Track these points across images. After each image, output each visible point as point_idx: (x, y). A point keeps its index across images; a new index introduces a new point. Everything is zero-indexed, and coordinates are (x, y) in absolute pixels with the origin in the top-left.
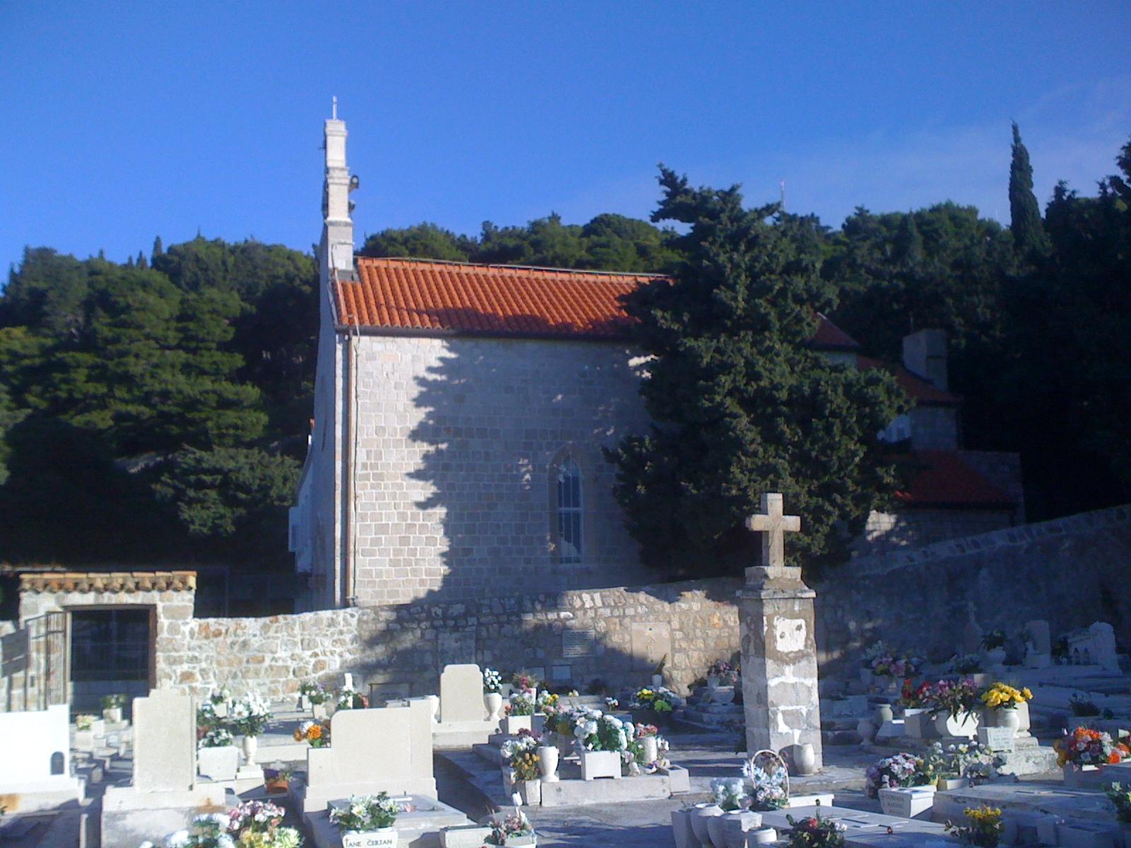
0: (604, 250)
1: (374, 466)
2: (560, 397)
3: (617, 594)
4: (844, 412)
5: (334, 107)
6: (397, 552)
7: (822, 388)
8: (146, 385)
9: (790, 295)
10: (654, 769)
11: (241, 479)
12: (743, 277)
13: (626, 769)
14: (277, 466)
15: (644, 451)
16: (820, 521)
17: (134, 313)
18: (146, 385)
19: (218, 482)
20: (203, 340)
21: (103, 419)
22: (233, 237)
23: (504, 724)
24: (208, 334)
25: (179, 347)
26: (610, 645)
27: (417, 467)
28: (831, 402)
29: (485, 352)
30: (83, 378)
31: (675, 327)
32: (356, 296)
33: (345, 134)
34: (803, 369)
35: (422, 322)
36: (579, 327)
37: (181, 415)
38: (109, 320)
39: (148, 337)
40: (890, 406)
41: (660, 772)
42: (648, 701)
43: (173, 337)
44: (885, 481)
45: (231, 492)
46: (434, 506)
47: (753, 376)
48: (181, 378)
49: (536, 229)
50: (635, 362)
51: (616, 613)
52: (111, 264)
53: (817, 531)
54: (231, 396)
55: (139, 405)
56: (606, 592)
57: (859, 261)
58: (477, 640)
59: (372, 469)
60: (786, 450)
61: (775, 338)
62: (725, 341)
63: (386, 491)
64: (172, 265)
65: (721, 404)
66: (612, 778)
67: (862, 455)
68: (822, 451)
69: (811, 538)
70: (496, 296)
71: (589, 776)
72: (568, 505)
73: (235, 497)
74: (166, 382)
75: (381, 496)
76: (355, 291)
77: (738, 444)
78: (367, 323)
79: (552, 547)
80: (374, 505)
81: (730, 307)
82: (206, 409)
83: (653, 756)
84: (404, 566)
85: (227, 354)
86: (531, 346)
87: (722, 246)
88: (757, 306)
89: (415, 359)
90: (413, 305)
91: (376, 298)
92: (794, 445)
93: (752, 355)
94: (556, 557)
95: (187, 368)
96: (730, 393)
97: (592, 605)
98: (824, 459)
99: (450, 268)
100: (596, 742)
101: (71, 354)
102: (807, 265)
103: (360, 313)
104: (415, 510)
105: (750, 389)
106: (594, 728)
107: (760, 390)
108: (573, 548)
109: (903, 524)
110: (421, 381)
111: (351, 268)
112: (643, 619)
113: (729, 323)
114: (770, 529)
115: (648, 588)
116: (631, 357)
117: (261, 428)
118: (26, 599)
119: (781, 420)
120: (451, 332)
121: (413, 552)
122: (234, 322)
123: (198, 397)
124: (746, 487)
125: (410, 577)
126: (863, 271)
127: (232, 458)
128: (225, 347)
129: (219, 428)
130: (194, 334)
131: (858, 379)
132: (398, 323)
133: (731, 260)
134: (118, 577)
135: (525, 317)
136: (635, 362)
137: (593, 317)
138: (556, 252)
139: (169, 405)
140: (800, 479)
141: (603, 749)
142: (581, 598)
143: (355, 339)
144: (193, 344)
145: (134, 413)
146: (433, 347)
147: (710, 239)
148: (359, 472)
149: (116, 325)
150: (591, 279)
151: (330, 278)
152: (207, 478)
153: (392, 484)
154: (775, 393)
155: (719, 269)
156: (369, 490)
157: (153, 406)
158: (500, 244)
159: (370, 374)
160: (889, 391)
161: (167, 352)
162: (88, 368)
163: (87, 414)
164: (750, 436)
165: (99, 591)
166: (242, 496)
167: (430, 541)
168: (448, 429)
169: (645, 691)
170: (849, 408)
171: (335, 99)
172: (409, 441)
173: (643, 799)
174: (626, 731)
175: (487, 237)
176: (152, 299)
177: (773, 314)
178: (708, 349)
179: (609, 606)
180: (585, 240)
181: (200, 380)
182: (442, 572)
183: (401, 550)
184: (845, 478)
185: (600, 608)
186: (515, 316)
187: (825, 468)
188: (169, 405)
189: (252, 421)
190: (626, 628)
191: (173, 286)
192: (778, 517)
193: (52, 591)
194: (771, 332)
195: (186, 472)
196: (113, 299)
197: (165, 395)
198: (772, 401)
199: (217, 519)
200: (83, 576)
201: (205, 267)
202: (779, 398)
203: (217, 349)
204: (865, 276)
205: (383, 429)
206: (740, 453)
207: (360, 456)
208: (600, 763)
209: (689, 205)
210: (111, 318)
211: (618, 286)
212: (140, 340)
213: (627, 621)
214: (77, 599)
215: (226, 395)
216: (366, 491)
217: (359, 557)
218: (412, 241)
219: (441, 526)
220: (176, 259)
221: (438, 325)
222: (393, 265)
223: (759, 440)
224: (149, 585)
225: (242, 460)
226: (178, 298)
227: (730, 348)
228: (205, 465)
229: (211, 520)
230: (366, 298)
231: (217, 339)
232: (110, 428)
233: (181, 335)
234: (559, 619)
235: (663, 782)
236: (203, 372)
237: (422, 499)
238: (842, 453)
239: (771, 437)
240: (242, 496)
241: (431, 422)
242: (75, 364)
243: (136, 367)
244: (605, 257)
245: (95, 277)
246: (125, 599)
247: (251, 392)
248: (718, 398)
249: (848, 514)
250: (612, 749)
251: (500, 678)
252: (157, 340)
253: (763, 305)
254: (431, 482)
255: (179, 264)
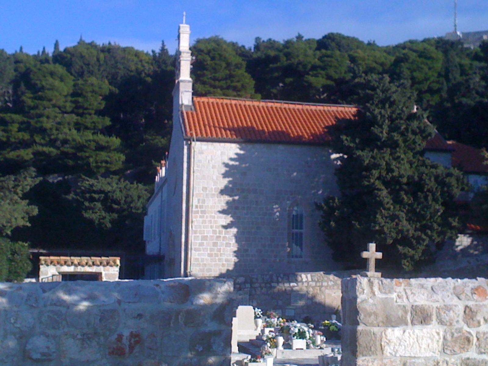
0: (329, 59)
1: (201, 207)
2: (295, 174)
3: (319, 275)
4: (434, 190)
5: (184, 17)
6: (211, 250)
7: (424, 177)
8: (53, 134)
9: (410, 130)
10: (319, 347)
11: (115, 197)
12: (387, 121)
13: (308, 346)
14: (135, 189)
15: (335, 205)
16: (420, 244)
17: (46, 91)
18: (53, 134)
19: (102, 198)
20: (86, 109)
21: (27, 154)
22: (101, 42)
23: (263, 331)
24: (90, 105)
25: (72, 112)
26: (317, 301)
27: (222, 208)
28: (428, 185)
29: (259, 150)
30: (16, 129)
31: (352, 145)
32: (193, 120)
33: (189, 32)
34: (417, 166)
35: (226, 134)
36: (305, 138)
37: (74, 154)
38: (32, 95)
39: (54, 106)
40: (457, 188)
41: (321, 348)
42: (327, 326)
43: (69, 106)
44: (453, 225)
45: (109, 204)
46: (231, 227)
47: (389, 170)
48: (74, 132)
49: (288, 45)
50: (334, 156)
51: (318, 284)
52: (27, 55)
53: (418, 248)
54: (104, 144)
55: (50, 147)
56: (314, 274)
57: (472, 86)
58: (250, 295)
59: (200, 208)
60: (405, 208)
61: (402, 151)
62: (376, 153)
63: (207, 219)
64: (66, 60)
65: (373, 184)
66: (302, 349)
67: (442, 211)
68: (422, 209)
69: (415, 251)
70: (263, 119)
71: (294, 348)
72: (297, 228)
73: (111, 207)
74: (66, 134)
75: (204, 222)
76: (193, 117)
77: (381, 204)
78: (200, 136)
79: (289, 249)
80: (201, 226)
81: (379, 136)
82: (89, 151)
83: (319, 342)
84: (215, 256)
85: (100, 117)
86: (281, 147)
87: (377, 105)
88: (392, 137)
89: (222, 153)
90: (222, 125)
91: (203, 120)
92: (409, 205)
93: (389, 159)
94: (290, 255)
95: (78, 127)
96: (379, 178)
97: (306, 280)
98: (423, 212)
99: (240, 102)
100: (297, 335)
101: (9, 115)
102: (419, 116)
103: (196, 130)
104: (221, 229)
105: (388, 176)
106: (297, 331)
107: (393, 177)
108: (298, 248)
109: (475, 243)
110: (226, 165)
111: (191, 104)
112: (332, 288)
113: (379, 143)
114: (369, 257)
115: (334, 272)
116: (332, 154)
117: (121, 163)
118: (43, 268)
119: (402, 193)
120: (241, 140)
121: (219, 250)
122: (105, 98)
123: (85, 144)
124: (383, 226)
125: (217, 262)
126: (474, 92)
127: (109, 184)
128: (100, 113)
129: (97, 162)
130: (81, 104)
131: (442, 174)
132: (215, 136)
133: (380, 113)
134: (85, 259)
135: (278, 132)
136: (334, 156)
137: (313, 132)
138: (299, 60)
139: (68, 148)
140: (411, 222)
141: (300, 338)
142: (301, 277)
143: (193, 143)
144: (81, 111)
145: (47, 152)
146: (231, 147)
147: (371, 102)
148: (194, 209)
149: (35, 98)
150: (314, 108)
151: (180, 109)
152: (96, 196)
153: (210, 216)
154: (400, 179)
155: (375, 117)
156: (198, 219)
157: (58, 148)
158: (265, 54)
159: (200, 161)
160: (458, 180)
161: (65, 115)
162: (19, 123)
163: (17, 151)
164: (386, 200)
165: (76, 266)
166: (116, 206)
167: (228, 245)
168: (238, 189)
169: (326, 322)
170: (436, 188)
171: (184, 13)
172: (219, 195)
173: (314, 358)
174: (309, 332)
175: (257, 47)
176: (57, 83)
177: (400, 140)
178: (367, 157)
179: (315, 281)
180: (318, 52)
181: (86, 133)
182: (233, 260)
183: (213, 249)
184: (433, 223)
185: (310, 281)
186: (273, 131)
187: (424, 217)
188: (68, 148)
189: (116, 159)
190: (323, 292)
191: (69, 74)
192: (373, 253)
193: (54, 265)
194: (400, 148)
195: (83, 192)
196: (33, 82)
197: (65, 142)
198: (398, 182)
199: (102, 219)
200: (68, 258)
201: (87, 63)
202: (402, 182)
203: (95, 114)
204: (475, 95)
205: (206, 188)
206: (382, 208)
207: (194, 201)
208: (298, 343)
209: (362, 84)
210: (33, 93)
211: (327, 112)
212: (49, 108)
213: (323, 289)
214: (66, 269)
215: (101, 142)
216: (197, 219)
217: (193, 252)
218: (213, 52)
219: (234, 238)
220: (69, 56)
221: (234, 137)
222: (211, 100)
223: (391, 202)
224: (99, 263)
225: (115, 186)
226: (72, 83)
227: (379, 156)
228: (94, 188)
229: (98, 220)
230: (198, 120)
231: (95, 108)
232: (31, 159)
233: (74, 105)
234: (290, 287)
235: (321, 352)
236: (86, 128)
237: (224, 224)
238: (432, 210)
239: (397, 201)
240: (116, 206)
241: (231, 186)
242: (11, 121)
243: (48, 124)
244: (330, 64)
245: (18, 64)
246: (88, 269)
247: (116, 141)
248: (372, 181)
249: (433, 241)
250: (303, 339)
251: (262, 312)
252: (59, 108)
253: (396, 136)
254: (229, 216)
255: (71, 59)
